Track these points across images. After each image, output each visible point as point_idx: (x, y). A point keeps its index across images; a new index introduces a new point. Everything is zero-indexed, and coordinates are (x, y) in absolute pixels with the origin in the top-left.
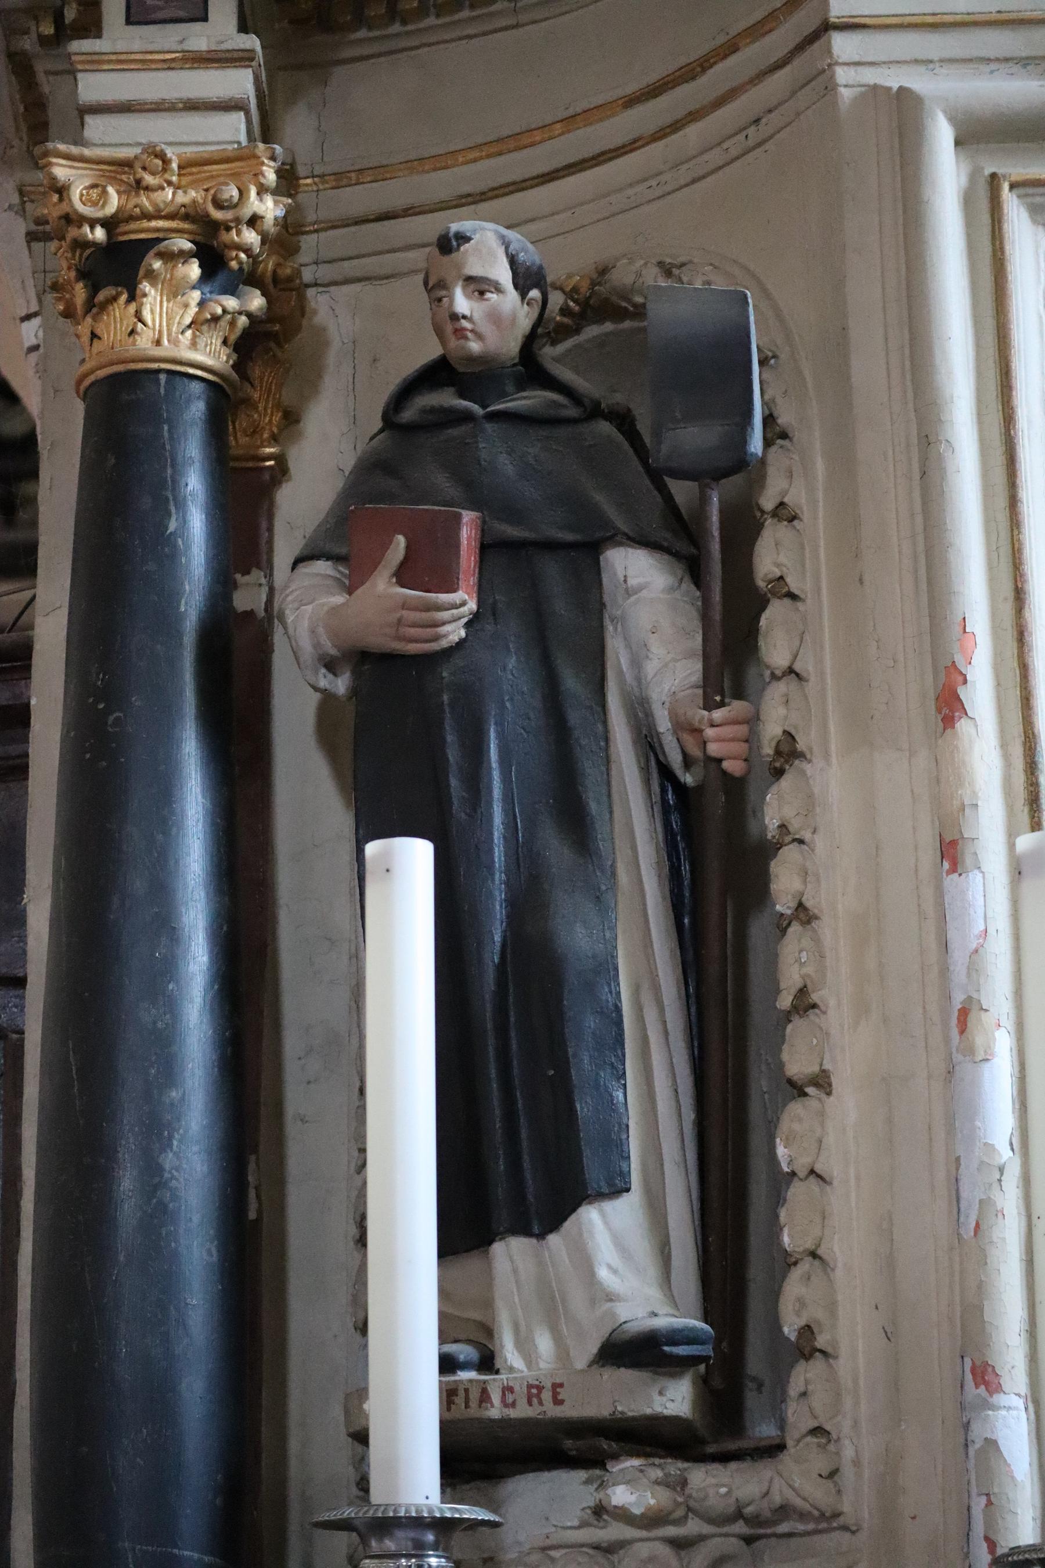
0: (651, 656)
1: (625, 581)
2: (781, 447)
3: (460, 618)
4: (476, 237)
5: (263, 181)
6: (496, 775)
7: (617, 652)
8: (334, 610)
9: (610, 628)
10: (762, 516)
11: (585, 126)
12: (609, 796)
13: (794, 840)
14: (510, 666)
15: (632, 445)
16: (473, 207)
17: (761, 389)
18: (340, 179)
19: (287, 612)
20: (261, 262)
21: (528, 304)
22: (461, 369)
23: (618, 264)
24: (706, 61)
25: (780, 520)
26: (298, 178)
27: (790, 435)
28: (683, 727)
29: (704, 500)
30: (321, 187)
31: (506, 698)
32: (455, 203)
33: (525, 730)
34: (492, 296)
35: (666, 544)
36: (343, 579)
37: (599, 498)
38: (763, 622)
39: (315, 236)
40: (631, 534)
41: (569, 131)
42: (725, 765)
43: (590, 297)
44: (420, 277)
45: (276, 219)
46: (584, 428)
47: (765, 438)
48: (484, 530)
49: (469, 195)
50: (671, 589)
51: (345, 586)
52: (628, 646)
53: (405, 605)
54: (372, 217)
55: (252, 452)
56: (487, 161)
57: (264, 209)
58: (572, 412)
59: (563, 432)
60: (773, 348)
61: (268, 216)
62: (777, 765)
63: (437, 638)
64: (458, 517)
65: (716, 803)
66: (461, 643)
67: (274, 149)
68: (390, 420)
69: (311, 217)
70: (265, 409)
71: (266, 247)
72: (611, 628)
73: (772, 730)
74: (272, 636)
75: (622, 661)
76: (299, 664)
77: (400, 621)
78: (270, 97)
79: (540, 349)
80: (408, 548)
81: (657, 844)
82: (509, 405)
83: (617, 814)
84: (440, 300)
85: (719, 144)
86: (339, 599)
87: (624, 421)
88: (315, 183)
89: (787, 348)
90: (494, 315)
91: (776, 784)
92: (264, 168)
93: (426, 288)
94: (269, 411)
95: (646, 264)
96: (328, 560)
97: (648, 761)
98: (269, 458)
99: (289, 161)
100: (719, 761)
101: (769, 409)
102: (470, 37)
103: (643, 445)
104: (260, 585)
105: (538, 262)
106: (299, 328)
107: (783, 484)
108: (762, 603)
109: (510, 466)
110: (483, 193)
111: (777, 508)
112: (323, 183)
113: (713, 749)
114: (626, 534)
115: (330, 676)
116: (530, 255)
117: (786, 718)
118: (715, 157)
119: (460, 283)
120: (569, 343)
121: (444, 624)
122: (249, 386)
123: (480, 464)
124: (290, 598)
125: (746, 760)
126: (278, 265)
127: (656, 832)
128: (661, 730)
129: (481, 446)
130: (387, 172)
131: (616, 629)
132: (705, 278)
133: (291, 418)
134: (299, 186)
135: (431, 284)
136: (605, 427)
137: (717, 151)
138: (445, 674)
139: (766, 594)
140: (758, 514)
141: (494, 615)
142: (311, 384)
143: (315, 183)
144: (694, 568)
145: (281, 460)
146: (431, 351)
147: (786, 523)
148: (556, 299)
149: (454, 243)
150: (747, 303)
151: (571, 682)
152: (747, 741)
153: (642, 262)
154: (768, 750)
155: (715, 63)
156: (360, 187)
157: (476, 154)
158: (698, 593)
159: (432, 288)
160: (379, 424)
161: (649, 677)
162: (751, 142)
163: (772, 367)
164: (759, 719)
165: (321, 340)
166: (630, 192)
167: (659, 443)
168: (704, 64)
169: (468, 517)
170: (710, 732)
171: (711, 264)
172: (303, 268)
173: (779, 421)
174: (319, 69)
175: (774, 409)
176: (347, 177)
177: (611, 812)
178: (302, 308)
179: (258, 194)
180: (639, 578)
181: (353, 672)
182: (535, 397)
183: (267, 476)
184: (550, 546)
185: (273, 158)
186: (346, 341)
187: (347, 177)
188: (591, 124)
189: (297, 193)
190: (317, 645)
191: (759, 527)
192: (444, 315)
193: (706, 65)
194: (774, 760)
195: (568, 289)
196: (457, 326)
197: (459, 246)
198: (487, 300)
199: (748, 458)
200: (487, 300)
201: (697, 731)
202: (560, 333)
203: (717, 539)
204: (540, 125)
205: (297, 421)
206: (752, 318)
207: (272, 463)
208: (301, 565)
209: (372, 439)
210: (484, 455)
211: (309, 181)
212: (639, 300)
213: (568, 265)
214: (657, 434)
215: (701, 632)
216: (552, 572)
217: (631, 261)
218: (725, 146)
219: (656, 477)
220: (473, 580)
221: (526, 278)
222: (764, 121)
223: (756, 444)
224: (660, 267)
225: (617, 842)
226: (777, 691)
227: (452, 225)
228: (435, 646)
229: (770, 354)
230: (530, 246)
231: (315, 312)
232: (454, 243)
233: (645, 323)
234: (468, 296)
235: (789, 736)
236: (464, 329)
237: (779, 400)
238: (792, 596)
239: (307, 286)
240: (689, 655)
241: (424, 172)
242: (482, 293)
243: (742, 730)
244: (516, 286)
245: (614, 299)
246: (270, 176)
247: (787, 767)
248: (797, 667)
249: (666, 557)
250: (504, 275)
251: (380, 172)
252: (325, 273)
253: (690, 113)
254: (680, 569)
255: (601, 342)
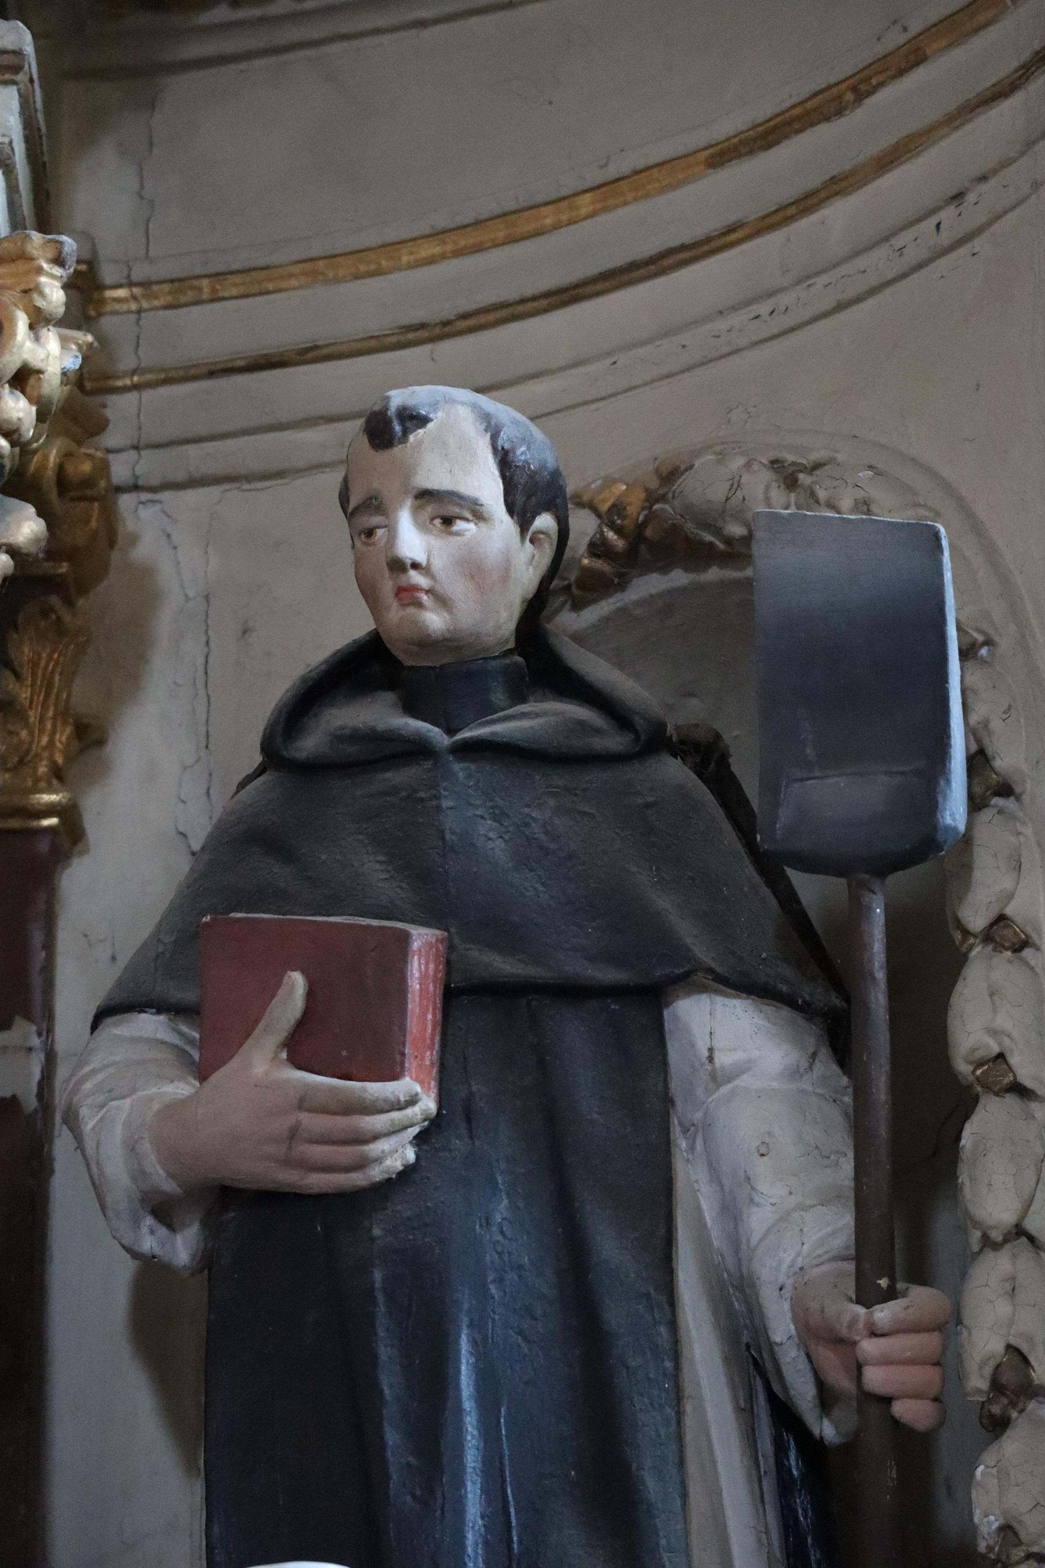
0: (757, 1199)
1: (711, 1059)
2: (1000, 812)
3: (406, 1128)
4: (438, 417)
5: (40, 303)
6: (471, 1423)
7: (694, 1184)
8: (172, 1109)
9: (681, 1143)
10: (964, 941)
11: (636, 199)
12: (681, 1463)
13: (1029, 1556)
14: (498, 1218)
15: (725, 805)
16: (427, 348)
17: (964, 704)
18: (183, 290)
19: (84, 1112)
20: (36, 451)
21: (532, 541)
22: (408, 662)
23: (697, 464)
24: (861, 82)
25: (999, 947)
26: (102, 287)
27: (1018, 789)
28: (815, 1333)
29: (858, 911)
30: (145, 305)
31: (490, 1278)
32: (394, 339)
33: (525, 1339)
34: (466, 527)
35: (784, 988)
36: (188, 1048)
37: (663, 903)
38: (967, 1140)
39: (132, 397)
40: (720, 970)
41: (606, 210)
42: (899, 1409)
43: (645, 523)
44: (334, 479)
45: (64, 374)
46: (634, 773)
47: (971, 797)
48: (450, 963)
49: (423, 326)
50: (794, 1074)
51: (193, 1063)
52: (715, 1175)
53: (305, 1103)
54: (240, 363)
55: (17, 801)
56: (455, 262)
57: (43, 356)
58: (615, 742)
59: (594, 778)
60: (985, 626)
61: (50, 369)
62: (996, 1409)
63: (362, 1164)
64: (404, 939)
65: (881, 1481)
66: (407, 1173)
67: (61, 243)
68: (275, 754)
69: (127, 362)
70: (42, 720)
71: (46, 426)
72: (684, 1145)
73: (984, 1344)
74: (51, 1145)
75: (704, 1206)
76: (103, 1208)
77: (294, 1134)
78: (48, 137)
79: (550, 619)
80: (311, 995)
81: (770, 1554)
82: (498, 728)
83: (695, 1490)
84: (370, 533)
85: (886, 239)
86: (182, 1088)
87: (708, 757)
88: (134, 298)
89: (1012, 627)
90: (469, 562)
91: (994, 1448)
92: (43, 279)
93: (345, 512)
94: (49, 725)
95: (748, 465)
96: (159, 1012)
97: (751, 1397)
98: (49, 811)
99: (86, 255)
100: (887, 1401)
101: (978, 741)
102: (422, 24)
103: (743, 801)
104: (30, 1049)
105: (551, 463)
106: (103, 570)
107: (1006, 883)
108: (962, 1103)
109: (500, 843)
110: (446, 323)
111: (992, 925)
112: (150, 296)
113: (875, 1378)
114: (710, 971)
115: (163, 1231)
116: (537, 449)
117: (1011, 1322)
118: (879, 262)
119: (409, 502)
120: (605, 607)
121: (376, 1137)
122: (12, 678)
123: (443, 838)
124: (88, 1085)
125: (936, 1399)
126: (68, 455)
127: (767, 1532)
128: (777, 1337)
129: (445, 804)
130: (269, 280)
131: (692, 1148)
132: (860, 494)
133: (90, 736)
134: (102, 301)
135: (353, 503)
136: (673, 771)
137: (881, 253)
138: (377, 1231)
139: (970, 1087)
140: (958, 936)
141: (469, 1120)
142: (127, 675)
143: (134, 298)
144: (837, 1034)
145: (71, 820)
146: (350, 624)
147: (1008, 954)
148: (584, 526)
149: (398, 428)
150: (940, 547)
151: (611, 1247)
152: (938, 1364)
153: (741, 461)
154: (978, 1382)
155: (881, 84)
156: (217, 306)
157: (431, 249)
158: (845, 1080)
159: (356, 510)
160: (258, 759)
161: (754, 1241)
162: (946, 237)
163: (983, 661)
164: (959, 1322)
165: (145, 589)
166: (721, 325)
167: (776, 805)
168: (861, 87)
169: (422, 938)
170: (869, 1347)
171: (871, 467)
172: (111, 457)
173: (997, 763)
174: (143, 78)
175: (986, 741)
176: (192, 288)
177: (684, 1496)
178: (110, 533)
179: (31, 327)
180: (734, 1045)
181: (204, 1224)
182: (544, 714)
183: (43, 846)
184: (572, 992)
185: (59, 261)
186: (191, 594)
187: (192, 288)
188: (647, 196)
189: (100, 315)
190: (139, 1174)
191: (960, 960)
192: (378, 560)
193: (863, 87)
194: (989, 1401)
195: (604, 507)
196: (403, 581)
197: (406, 433)
198: (458, 534)
199: (940, 837)
200: (458, 534)
201: (843, 1344)
202: (591, 588)
203: (882, 985)
204: (553, 196)
205: (100, 743)
206: (948, 576)
207: (52, 821)
208: (110, 1020)
209: (242, 785)
210: (451, 823)
211: (121, 293)
212: (736, 530)
213: (606, 460)
214: (772, 787)
215: (851, 1155)
216: (576, 1040)
217: (722, 457)
218: (898, 242)
219: (770, 866)
220: (430, 1056)
221: (530, 493)
222: (971, 197)
223: (954, 810)
224: (776, 471)
225: (696, 1552)
226: (993, 1270)
227: (392, 393)
228: (358, 1179)
229: (980, 638)
230: (533, 428)
231: (134, 539)
232: (398, 428)
233: (749, 572)
234: (422, 527)
235: (1017, 1355)
236: (416, 588)
237: (996, 724)
238: (1020, 1090)
239: (119, 490)
240: (827, 1198)
241: (338, 281)
242: (448, 521)
243: (930, 1342)
244: (510, 508)
245: (690, 527)
246: (54, 294)
247: (1014, 1415)
248: (1032, 1225)
249: (786, 1012)
250: (487, 486)
251: (257, 280)
252: (149, 466)
253: (833, 180)
254: (811, 1035)
255: (667, 604)
